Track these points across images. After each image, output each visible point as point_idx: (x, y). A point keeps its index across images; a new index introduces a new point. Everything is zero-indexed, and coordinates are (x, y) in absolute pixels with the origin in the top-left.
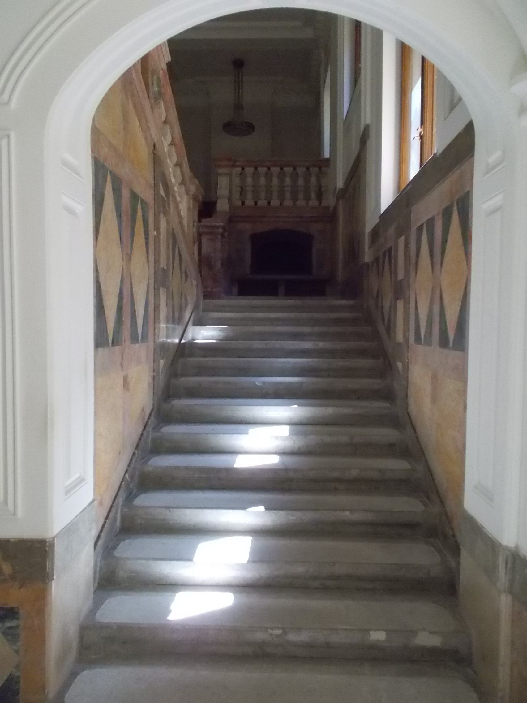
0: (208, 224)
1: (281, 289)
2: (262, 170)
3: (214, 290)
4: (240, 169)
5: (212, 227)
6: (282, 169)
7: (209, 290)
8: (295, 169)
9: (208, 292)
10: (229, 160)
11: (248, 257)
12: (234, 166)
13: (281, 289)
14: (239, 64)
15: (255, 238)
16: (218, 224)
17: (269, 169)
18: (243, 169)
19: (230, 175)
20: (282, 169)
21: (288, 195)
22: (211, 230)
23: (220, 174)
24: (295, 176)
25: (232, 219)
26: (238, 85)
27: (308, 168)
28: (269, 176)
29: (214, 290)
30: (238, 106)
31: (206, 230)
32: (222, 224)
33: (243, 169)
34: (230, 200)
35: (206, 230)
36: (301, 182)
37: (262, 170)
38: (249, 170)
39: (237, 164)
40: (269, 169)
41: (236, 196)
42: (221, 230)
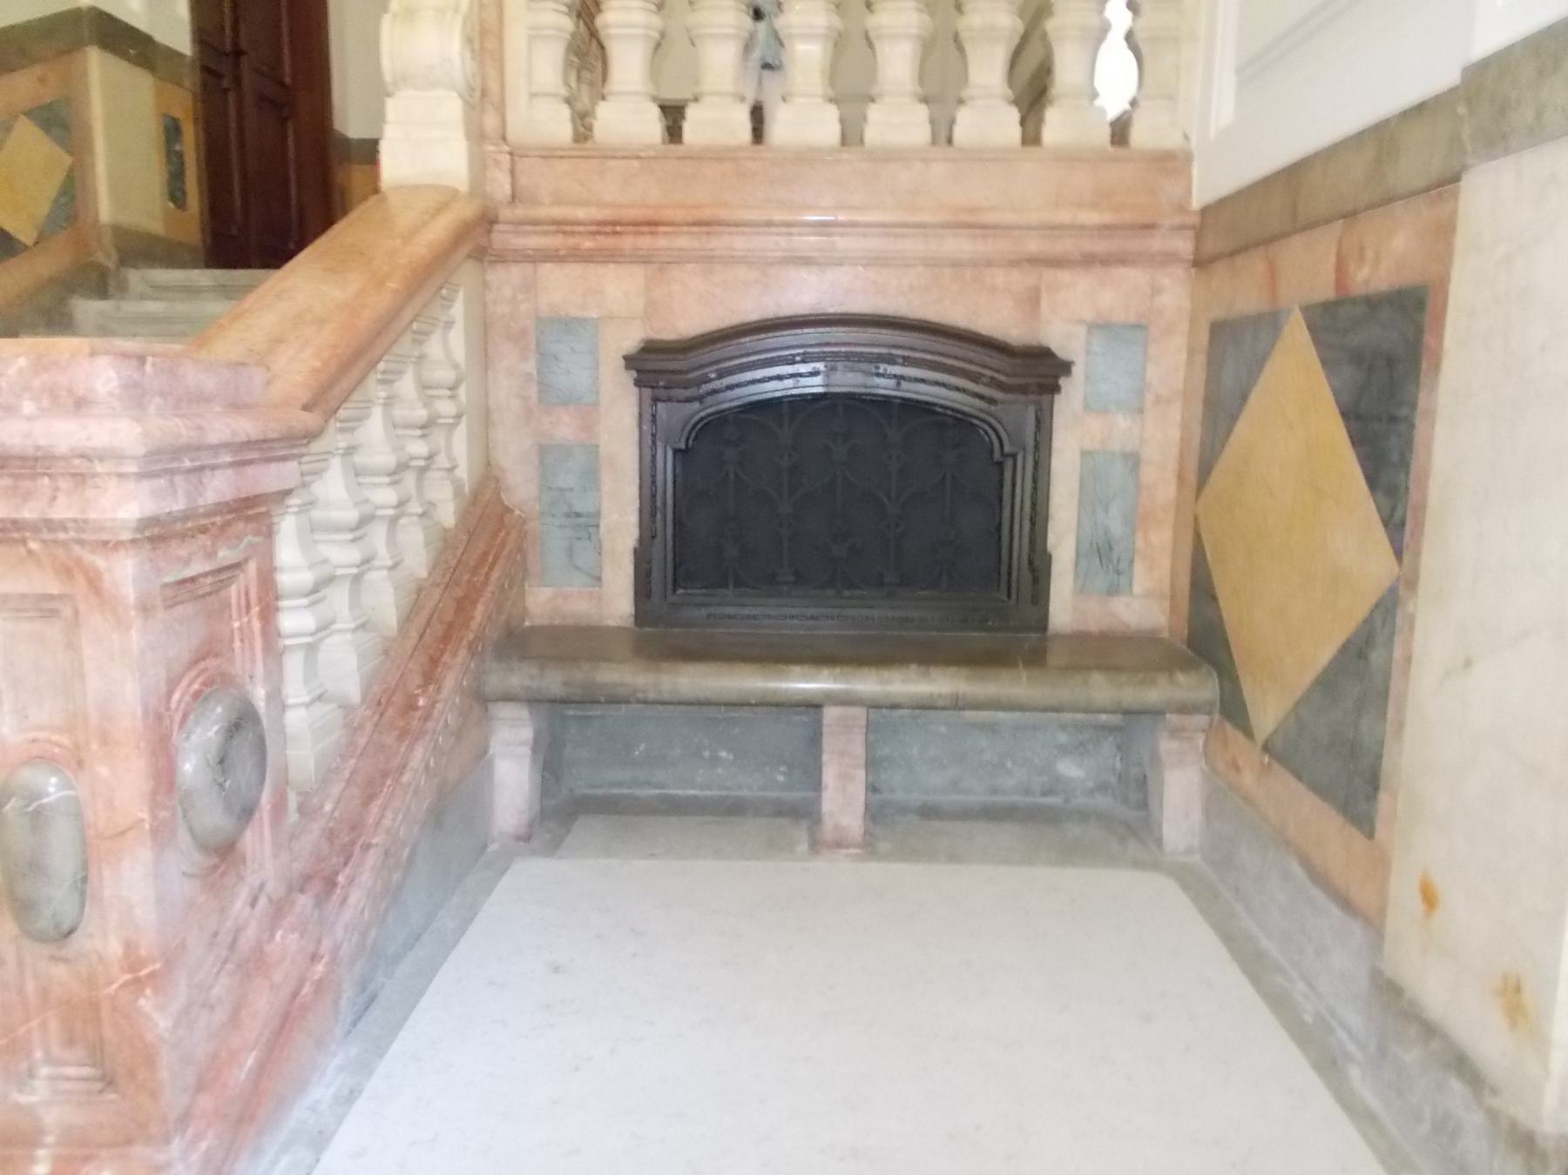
15: (658, 368)
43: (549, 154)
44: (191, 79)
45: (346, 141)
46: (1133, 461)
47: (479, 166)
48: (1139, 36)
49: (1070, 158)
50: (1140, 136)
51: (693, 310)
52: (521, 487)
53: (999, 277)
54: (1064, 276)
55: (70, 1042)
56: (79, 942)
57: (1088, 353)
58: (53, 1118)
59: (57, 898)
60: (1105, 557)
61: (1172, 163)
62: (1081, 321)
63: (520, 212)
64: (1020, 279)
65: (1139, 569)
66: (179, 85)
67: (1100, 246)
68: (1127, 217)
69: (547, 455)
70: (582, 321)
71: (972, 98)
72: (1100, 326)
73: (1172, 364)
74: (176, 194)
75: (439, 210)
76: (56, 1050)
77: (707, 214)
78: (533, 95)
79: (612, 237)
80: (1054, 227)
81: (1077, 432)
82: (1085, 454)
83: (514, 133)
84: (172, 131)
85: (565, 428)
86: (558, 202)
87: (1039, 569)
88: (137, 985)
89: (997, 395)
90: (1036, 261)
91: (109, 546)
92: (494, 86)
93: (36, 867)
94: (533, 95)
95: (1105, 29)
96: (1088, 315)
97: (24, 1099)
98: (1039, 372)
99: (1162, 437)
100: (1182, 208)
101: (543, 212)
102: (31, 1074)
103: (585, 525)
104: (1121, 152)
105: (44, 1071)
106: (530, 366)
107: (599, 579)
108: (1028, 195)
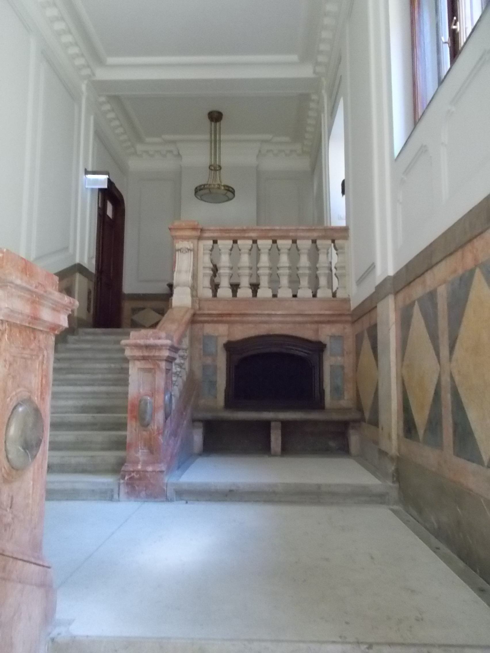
0: (141, 342)
1: (276, 439)
2: (245, 244)
3: (150, 469)
4: (211, 242)
5: (148, 347)
6: (274, 242)
7: (140, 467)
8: (294, 242)
9: (138, 472)
10: (194, 229)
11: (221, 381)
12: (200, 238)
13: (276, 439)
14: (215, 117)
15: (231, 347)
16: (159, 342)
17: (255, 242)
18: (215, 242)
19: (195, 252)
20: (274, 242)
21: (284, 281)
22: (146, 354)
23: (179, 250)
24: (294, 253)
25: (195, 319)
26: (215, 143)
27: (314, 242)
28: (255, 252)
29: (150, 469)
30: (215, 168)
31: (137, 353)
32: (168, 342)
33: (215, 242)
34: (194, 288)
35: (137, 353)
36: (304, 261)
37: (245, 244)
38: (225, 244)
39: (206, 235)
40: (255, 242)
41: (205, 282)
42: (166, 353)
43: (207, 300)
44: (94, 279)
45: (124, 294)
46: (342, 367)
47: (193, 302)
48: (337, 275)
49: (324, 300)
50: (339, 295)
51: (240, 333)
52: (198, 374)
53: (309, 326)
54: (324, 325)
55: (145, 446)
56: (149, 427)
57: (330, 342)
58: (141, 458)
59: (148, 418)
60: (337, 391)
61: (347, 301)
62: (328, 335)
63: (201, 312)
64: (314, 326)
65: (346, 394)
66: (91, 280)
67: (334, 319)
68: (336, 312)
69: (205, 367)
70: (212, 336)
71: (301, 288)
72: (332, 337)
73: (349, 344)
74: (88, 309)
75: (186, 312)
76: (142, 447)
77: (243, 312)
78: (203, 287)
79: (220, 318)
80: (321, 315)
81: (329, 362)
82: (331, 366)
83: (199, 294)
84: (89, 293)
85: (209, 361)
86: (209, 309)
87: (322, 393)
88: (159, 434)
89: (310, 352)
90: (317, 322)
91: (161, 360)
92: (195, 286)
93: (145, 412)
94: (203, 287)
95: (39, 442)
96: (330, 334)
97: (137, 455)
98: (319, 348)
99: (348, 361)
100: (349, 310)
101: (206, 312)
102: (138, 451)
103: (213, 384)
104: (335, 299)
105: (140, 451)
106: (201, 347)
107: (216, 397)
108: (315, 309)
